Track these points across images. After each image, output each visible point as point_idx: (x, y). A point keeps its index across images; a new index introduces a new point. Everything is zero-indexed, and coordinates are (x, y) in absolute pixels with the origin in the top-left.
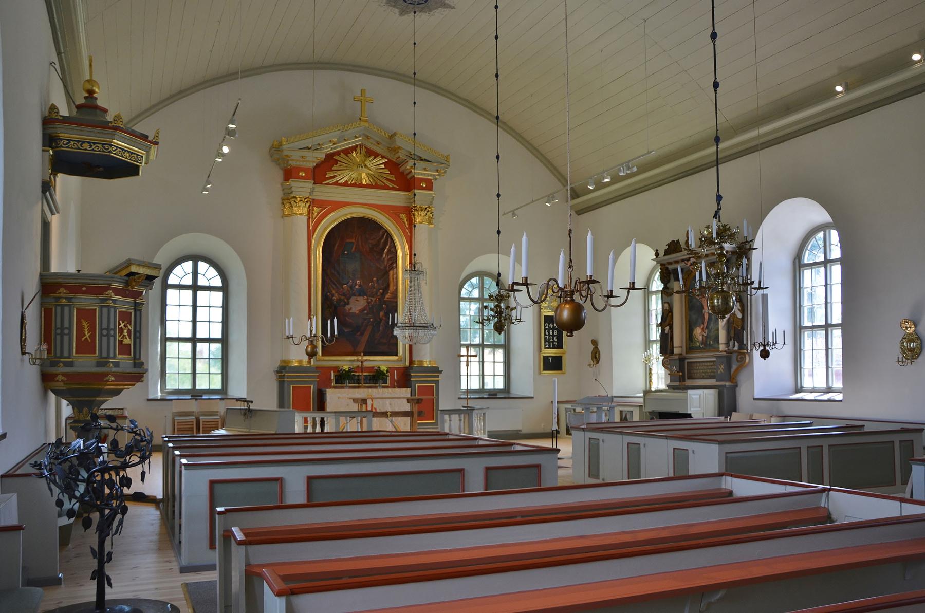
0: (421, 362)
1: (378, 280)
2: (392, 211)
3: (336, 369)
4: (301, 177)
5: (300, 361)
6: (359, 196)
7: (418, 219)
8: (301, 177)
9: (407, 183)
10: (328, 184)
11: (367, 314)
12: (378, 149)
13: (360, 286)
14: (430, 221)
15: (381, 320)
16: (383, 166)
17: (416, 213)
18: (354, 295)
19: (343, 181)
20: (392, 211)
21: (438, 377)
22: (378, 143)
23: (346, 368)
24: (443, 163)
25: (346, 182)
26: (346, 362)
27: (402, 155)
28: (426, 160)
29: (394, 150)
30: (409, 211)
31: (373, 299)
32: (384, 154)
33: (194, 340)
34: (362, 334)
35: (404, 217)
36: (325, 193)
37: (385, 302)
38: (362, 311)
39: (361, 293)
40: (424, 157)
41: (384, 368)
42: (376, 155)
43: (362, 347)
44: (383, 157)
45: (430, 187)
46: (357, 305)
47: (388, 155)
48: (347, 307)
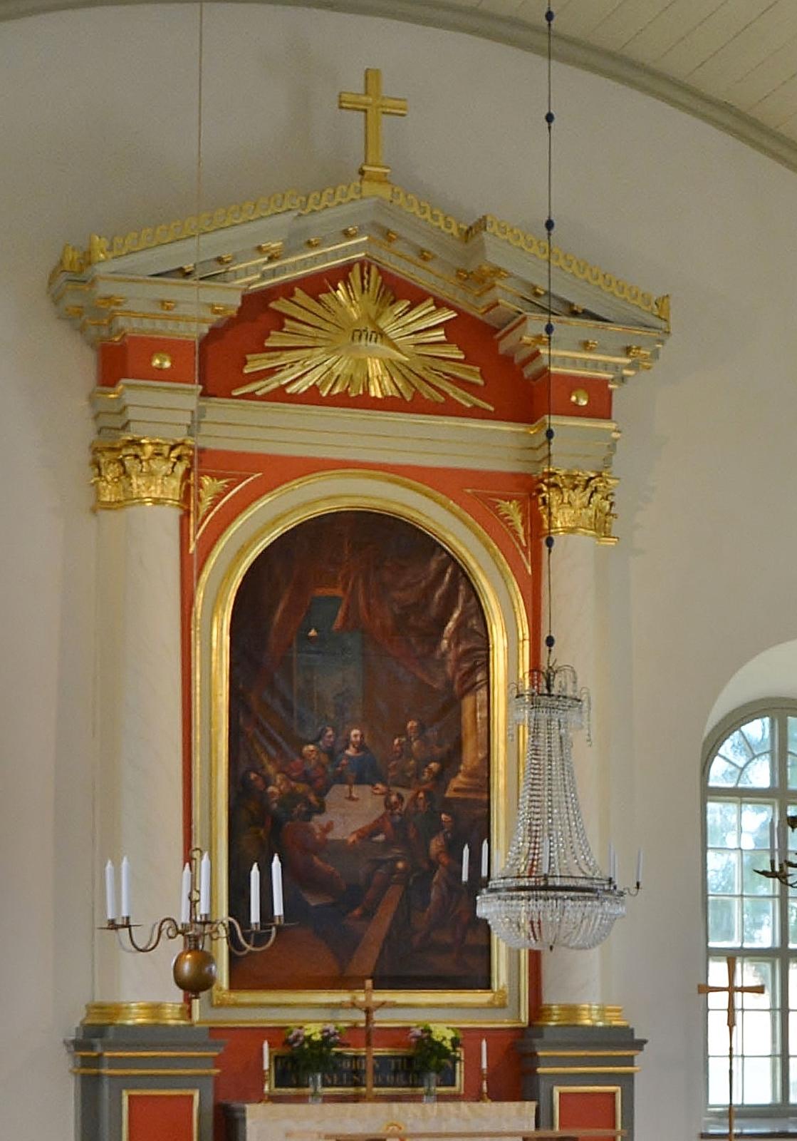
0: (572, 1010)
1: (422, 728)
2: (472, 490)
3: (278, 1034)
4: (160, 374)
5: (156, 1009)
6: (358, 439)
7: (561, 519)
8: (160, 374)
9: (523, 394)
10: (250, 396)
11: (387, 844)
12: (422, 278)
13: (361, 747)
14: (601, 526)
15: (433, 865)
16: (439, 335)
17: (554, 497)
18: (340, 779)
19: (301, 387)
20: (472, 490)
21: (629, 1061)
22: (423, 255)
23: (314, 1031)
24: (649, 324)
25: (314, 389)
26: (312, 1012)
27: (506, 297)
28: (588, 315)
29: (480, 279)
30: (530, 489)
31: (407, 794)
32: (445, 294)
33: (743, 1056)
34: (369, 914)
35: (512, 509)
36: (240, 426)
37: (448, 805)
38: (366, 835)
39: (366, 773)
40: (580, 304)
41: (443, 1033)
42: (416, 297)
43: (367, 958)
44: (440, 304)
45: (601, 407)
46: (350, 815)
47: (459, 298)
48: (318, 821)
